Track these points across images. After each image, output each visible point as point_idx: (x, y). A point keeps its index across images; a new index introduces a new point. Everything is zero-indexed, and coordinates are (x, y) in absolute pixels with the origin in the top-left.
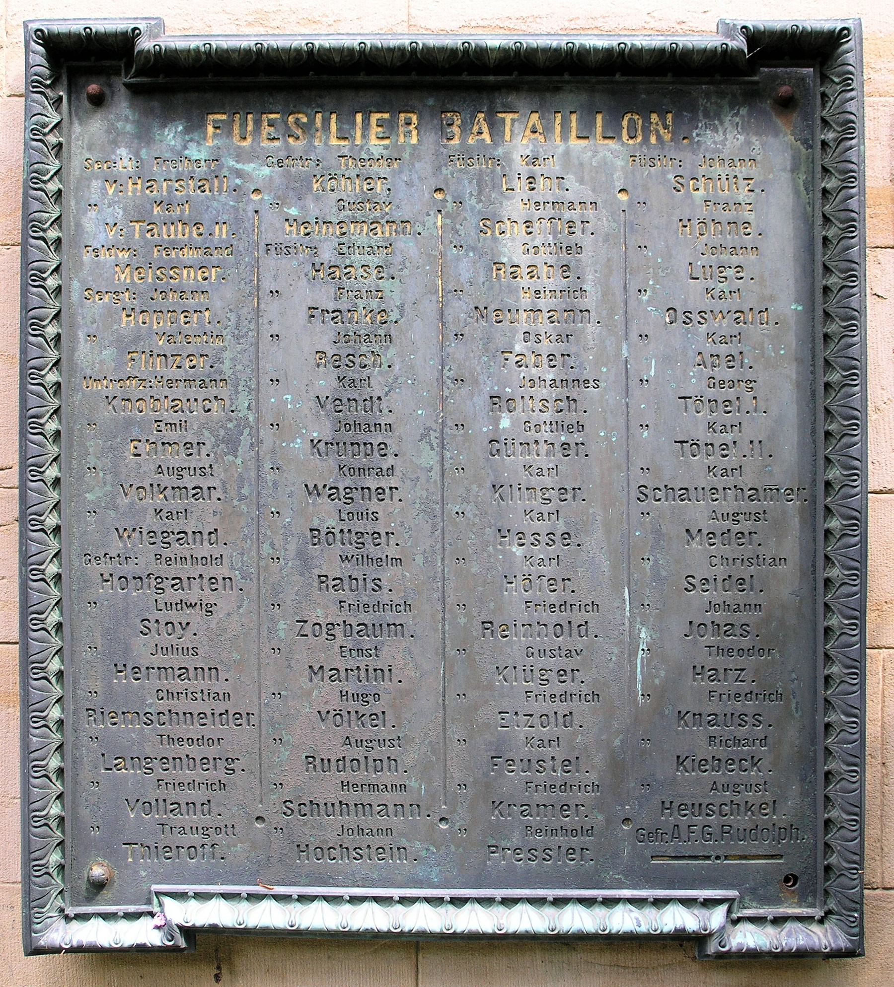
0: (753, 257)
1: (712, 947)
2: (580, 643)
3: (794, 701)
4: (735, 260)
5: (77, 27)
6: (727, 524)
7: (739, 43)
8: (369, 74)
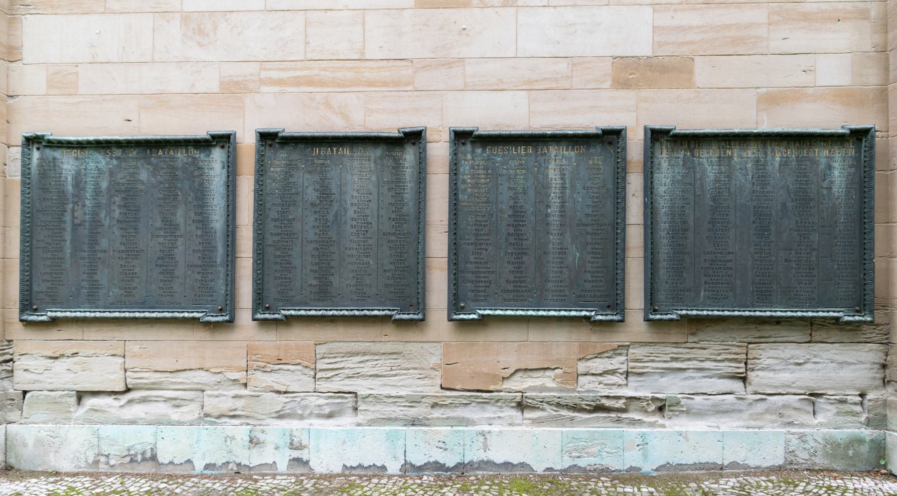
1: (592, 319)
2: (564, 256)
5: (461, 129)
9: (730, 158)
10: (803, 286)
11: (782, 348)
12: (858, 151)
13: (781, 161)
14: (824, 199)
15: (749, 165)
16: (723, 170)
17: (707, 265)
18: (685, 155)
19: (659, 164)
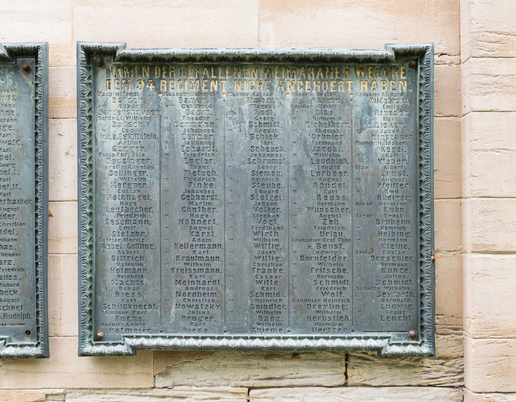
0: (15, 123)
1: (383, 352)
3: (28, 271)
4: (9, 124)
6: (5, 212)
7: (391, 53)
8: (176, 62)
9: (216, 94)
10: (329, 297)
11: (301, 395)
12: (412, 84)
13: (294, 100)
14: (361, 160)
15: (245, 107)
16: (205, 114)
17: (181, 264)
18: (145, 90)
19: (105, 105)
